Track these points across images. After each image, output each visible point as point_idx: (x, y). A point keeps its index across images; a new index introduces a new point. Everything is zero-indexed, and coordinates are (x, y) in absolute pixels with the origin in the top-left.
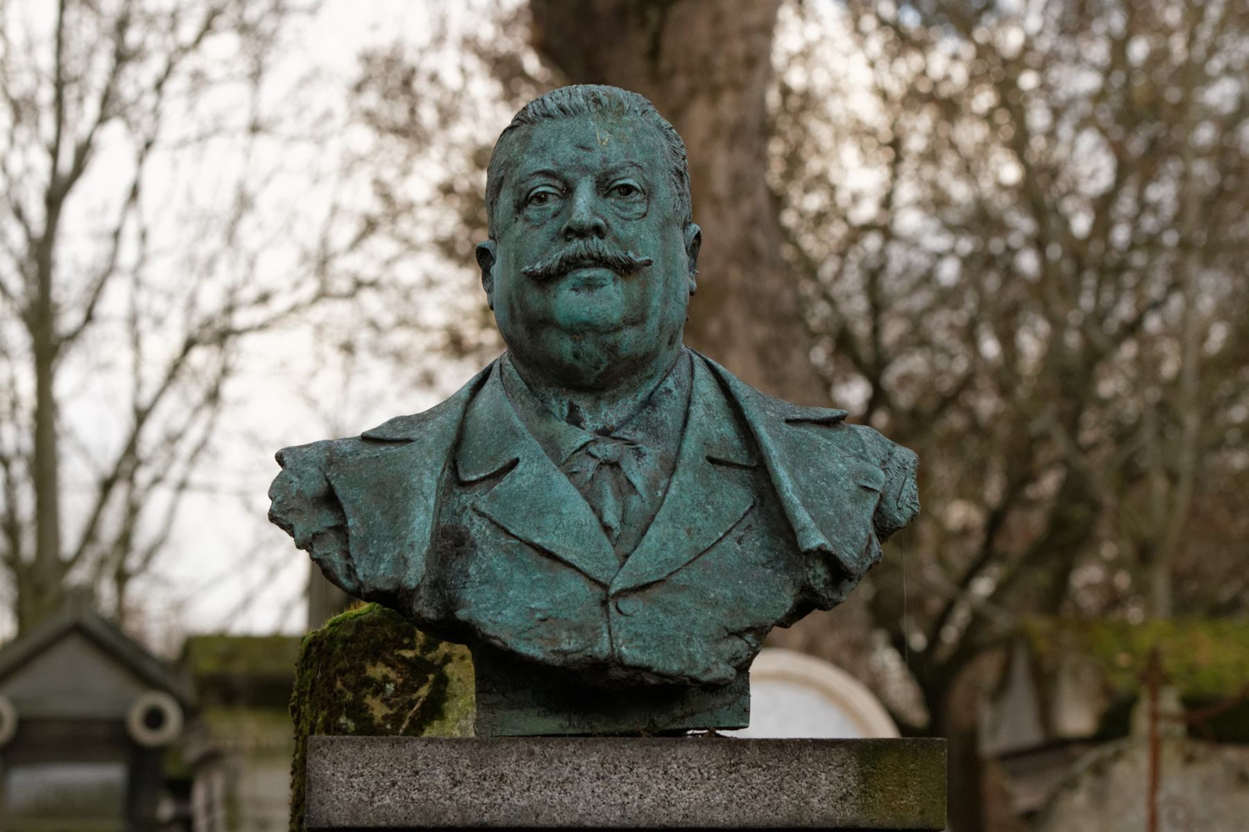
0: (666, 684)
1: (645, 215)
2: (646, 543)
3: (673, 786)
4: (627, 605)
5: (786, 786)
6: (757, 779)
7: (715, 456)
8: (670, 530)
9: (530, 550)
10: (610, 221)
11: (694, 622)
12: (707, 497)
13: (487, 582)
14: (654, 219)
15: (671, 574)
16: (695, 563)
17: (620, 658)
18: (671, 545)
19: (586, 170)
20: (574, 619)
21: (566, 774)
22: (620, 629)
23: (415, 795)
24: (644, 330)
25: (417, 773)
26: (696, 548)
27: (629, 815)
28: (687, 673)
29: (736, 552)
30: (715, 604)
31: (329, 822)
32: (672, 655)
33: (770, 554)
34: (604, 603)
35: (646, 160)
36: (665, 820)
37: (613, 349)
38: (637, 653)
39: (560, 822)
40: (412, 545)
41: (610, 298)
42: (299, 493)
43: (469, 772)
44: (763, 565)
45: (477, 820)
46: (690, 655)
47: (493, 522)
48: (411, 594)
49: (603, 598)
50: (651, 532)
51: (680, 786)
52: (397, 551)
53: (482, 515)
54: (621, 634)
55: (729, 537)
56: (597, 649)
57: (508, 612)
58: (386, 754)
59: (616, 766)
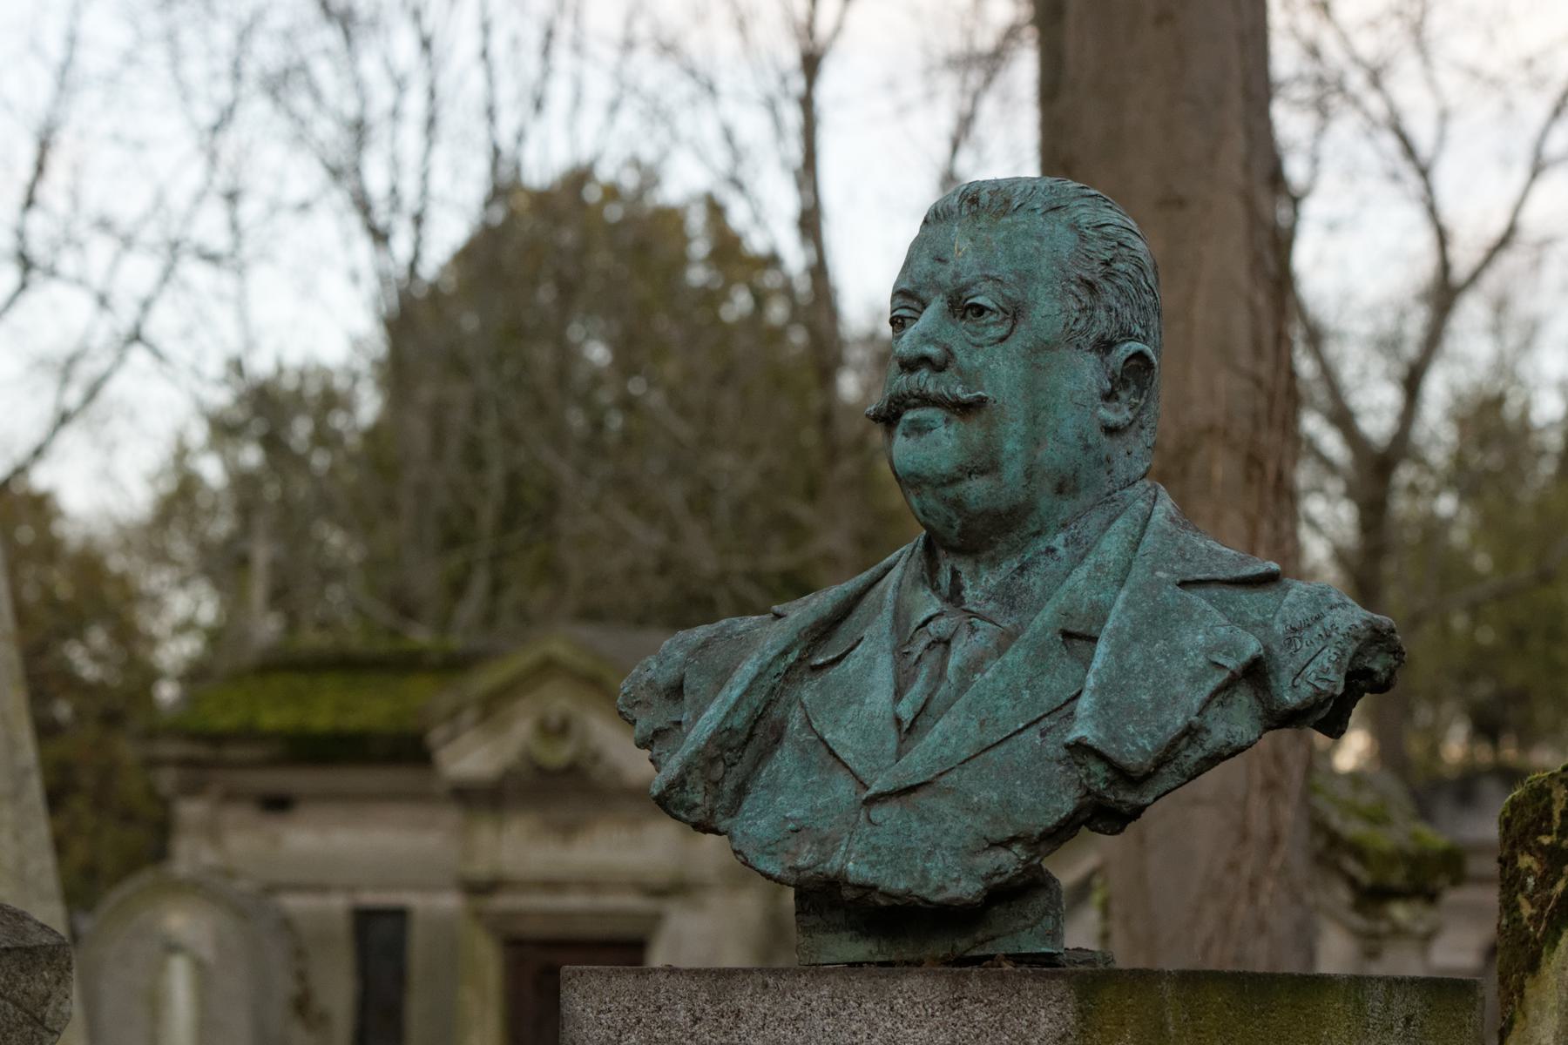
1: (1003, 339)
5: (1007, 1024)
6: (980, 1016)
7: (1071, 629)
10: (956, 349)
12: (1031, 679)
14: (1015, 344)
16: (974, 761)
19: (939, 287)
21: (798, 1010)
24: (1000, 480)
28: (915, 892)
30: (977, 810)
32: (903, 872)
35: (1013, 272)
37: (957, 504)
41: (937, 444)
42: (650, 683)
55: (1033, 729)
58: (631, 987)
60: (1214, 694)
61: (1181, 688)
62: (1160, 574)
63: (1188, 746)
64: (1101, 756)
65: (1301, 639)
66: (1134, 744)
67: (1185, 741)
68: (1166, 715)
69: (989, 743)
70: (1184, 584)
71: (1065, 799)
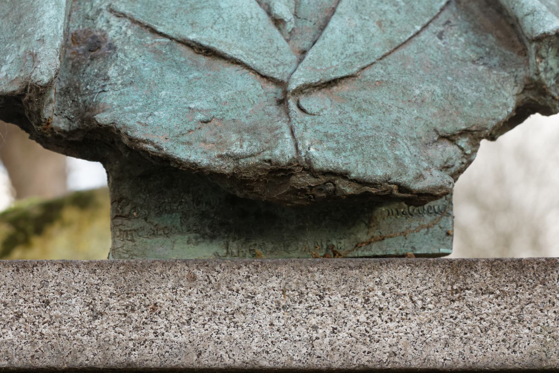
0: (367, 194)
2: (328, 35)
3: (376, 318)
4: (312, 102)
5: (527, 317)
8: (358, 22)
9: (183, 48)
11: (397, 122)
13: (131, 83)
15: (363, 68)
16: (391, 57)
17: (308, 161)
18: (360, 37)
20: (244, 119)
22: (306, 129)
23: (46, 330)
25: (47, 303)
26: (391, 41)
27: (318, 352)
28: (394, 179)
29: (439, 48)
31: (278, 109)
32: (375, 159)
33: (479, 50)
34: (282, 102)
36: (365, 360)
38: (329, 155)
39: (228, 362)
40: (42, 40)
43: (113, 302)
44: (473, 62)
45: (122, 359)
46: (396, 158)
47: (134, 22)
48: (40, 91)
49: (280, 96)
50: (334, 23)
51: (385, 317)
52: (23, 49)
53: (121, 15)
54: (307, 134)
55: (427, 32)
56: (277, 152)
57: (162, 114)
58: (9, 280)
59: (301, 294)
69: (398, 42)
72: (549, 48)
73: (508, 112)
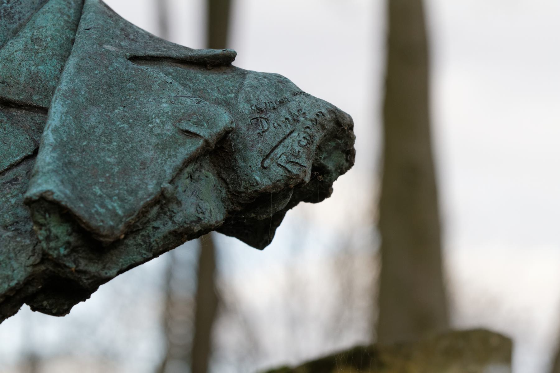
60: (187, 163)
61: (148, 155)
62: (107, 47)
63: (158, 216)
64: (65, 214)
65: (267, 119)
66: (103, 206)
67: (155, 210)
68: (135, 180)
70: (134, 58)
71: (16, 265)
72: (45, 213)
73: (9, 285)
